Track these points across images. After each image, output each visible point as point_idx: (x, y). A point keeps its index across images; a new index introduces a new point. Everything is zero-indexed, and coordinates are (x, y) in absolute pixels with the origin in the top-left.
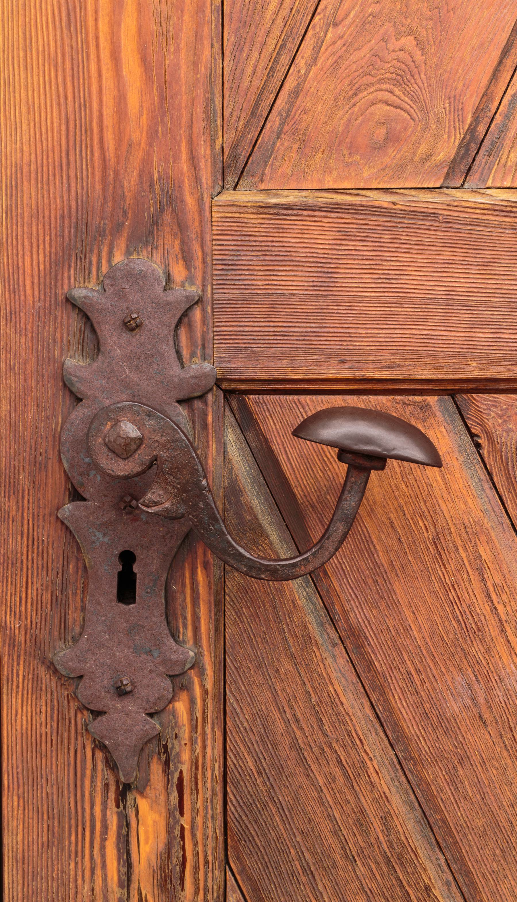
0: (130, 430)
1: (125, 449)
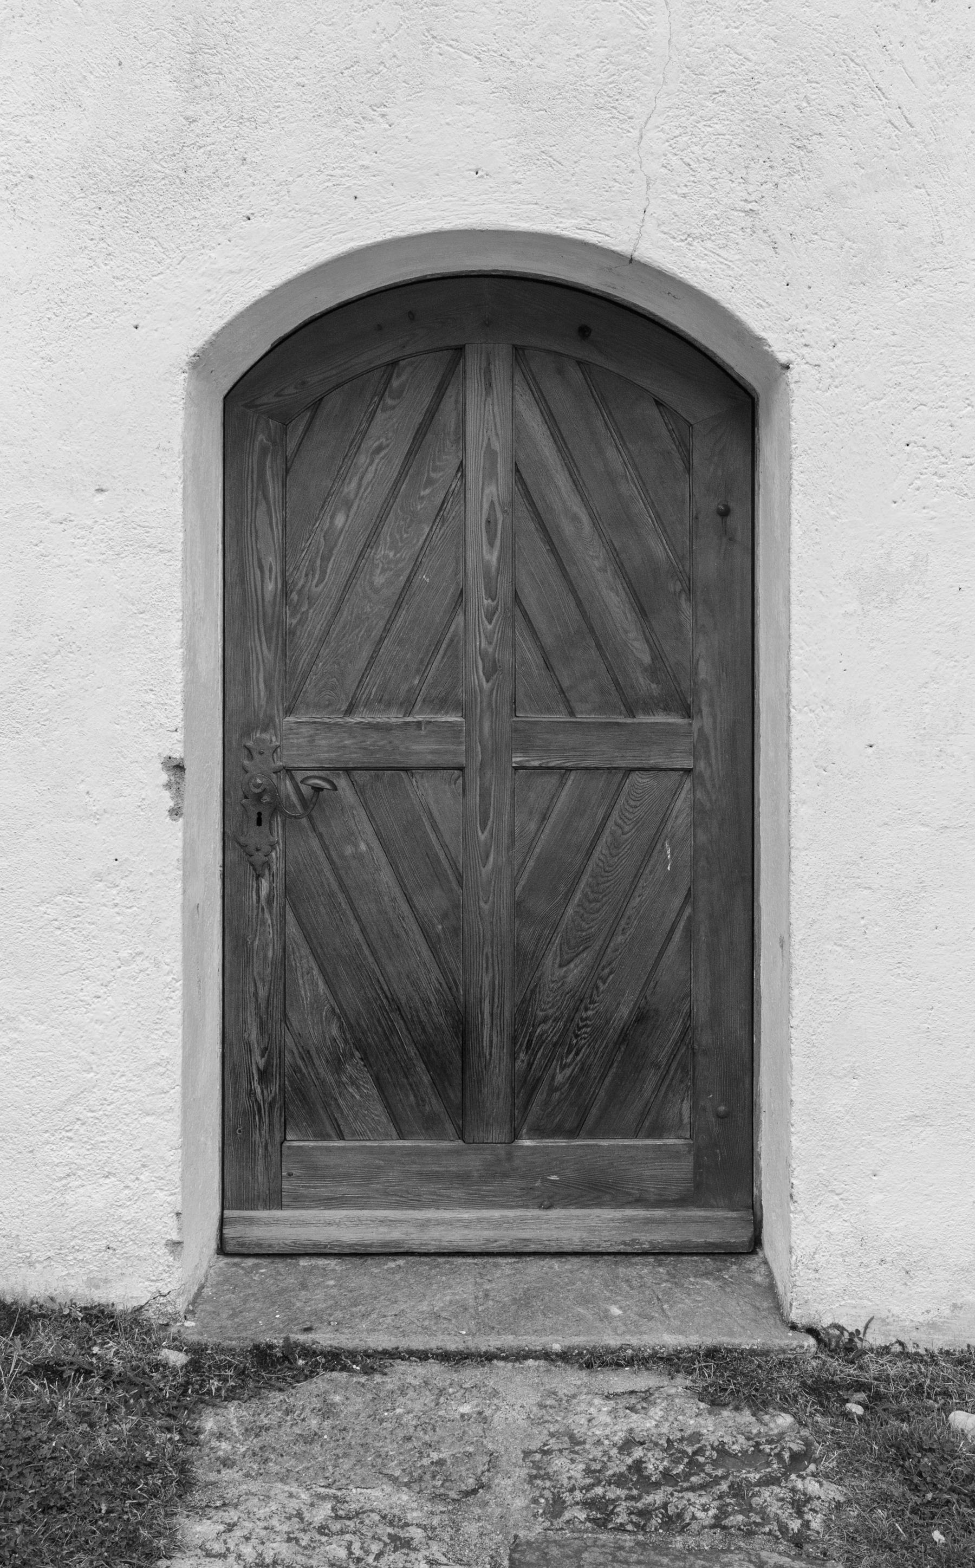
0: (259, 781)
1: (258, 786)
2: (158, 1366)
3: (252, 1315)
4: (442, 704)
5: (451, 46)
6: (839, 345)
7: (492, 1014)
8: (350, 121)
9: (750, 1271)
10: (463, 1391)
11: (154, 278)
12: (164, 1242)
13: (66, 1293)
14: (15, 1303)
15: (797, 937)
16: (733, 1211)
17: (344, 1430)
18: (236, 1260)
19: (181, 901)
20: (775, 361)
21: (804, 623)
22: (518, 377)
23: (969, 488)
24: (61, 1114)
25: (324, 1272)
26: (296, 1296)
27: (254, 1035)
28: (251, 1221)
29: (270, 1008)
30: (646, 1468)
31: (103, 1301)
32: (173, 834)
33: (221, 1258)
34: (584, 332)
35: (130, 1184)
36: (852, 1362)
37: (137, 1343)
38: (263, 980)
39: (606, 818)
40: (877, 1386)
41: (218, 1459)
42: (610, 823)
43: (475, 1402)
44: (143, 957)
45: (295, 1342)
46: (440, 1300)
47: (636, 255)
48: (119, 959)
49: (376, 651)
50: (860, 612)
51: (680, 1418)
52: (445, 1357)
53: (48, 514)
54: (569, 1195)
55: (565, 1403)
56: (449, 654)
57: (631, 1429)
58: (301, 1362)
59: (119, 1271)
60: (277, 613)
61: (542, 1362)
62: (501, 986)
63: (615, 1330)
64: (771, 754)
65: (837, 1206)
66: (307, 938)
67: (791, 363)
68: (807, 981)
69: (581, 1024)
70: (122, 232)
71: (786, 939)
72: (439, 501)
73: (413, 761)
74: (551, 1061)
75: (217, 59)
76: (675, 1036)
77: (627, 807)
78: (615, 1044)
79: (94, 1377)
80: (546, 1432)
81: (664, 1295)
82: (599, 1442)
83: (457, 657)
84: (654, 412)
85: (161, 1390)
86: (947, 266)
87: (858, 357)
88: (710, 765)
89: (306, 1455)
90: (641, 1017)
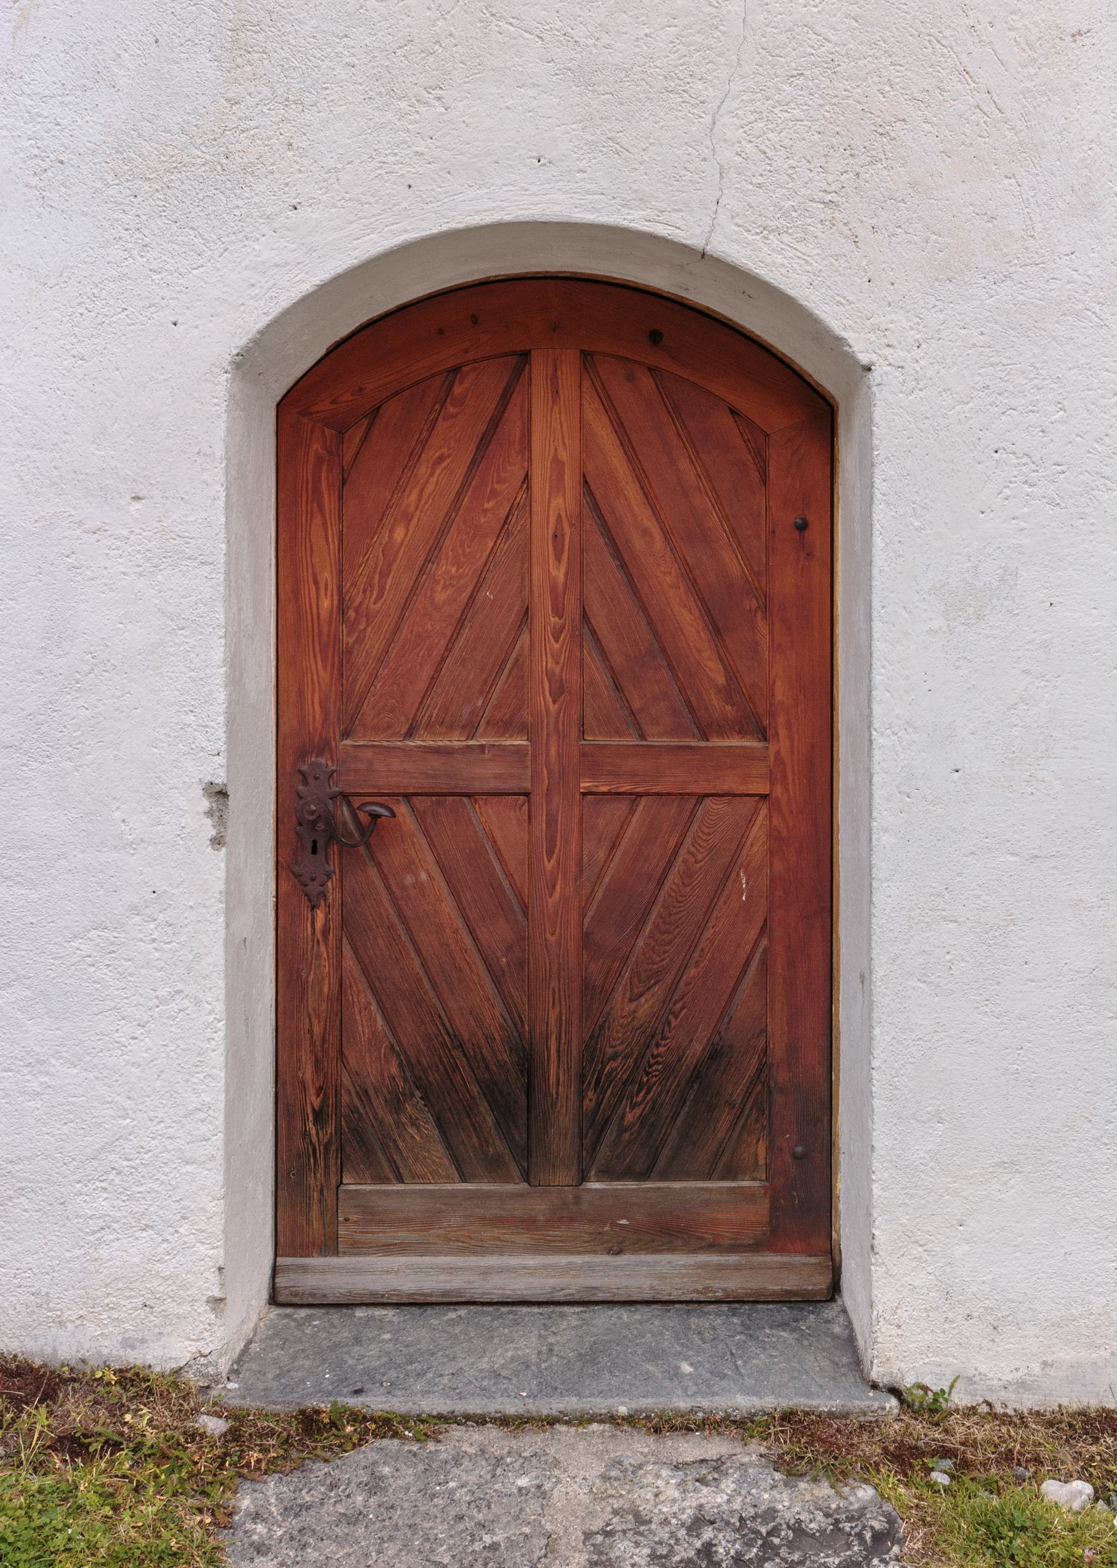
0: (313, 808)
1: (313, 812)
2: (193, 1436)
3: (300, 1374)
4: (506, 726)
5: (511, 24)
6: (924, 346)
7: (558, 1051)
8: (403, 105)
9: (828, 1321)
10: (521, 1460)
11: (194, 272)
12: (205, 1298)
13: (100, 1354)
14: (44, 1365)
15: (879, 973)
16: (810, 1256)
17: (392, 1507)
18: (289, 1311)
19: (224, 936)
20: (856, 362)
21: (886, 641)
22: (587, 384)
23: (1062, 498)
24: (95, 1163)
25: (381, 1324)
26: (348, 1353)
27: (308, 1073)
28: (305, 1269)
29: (326, 1046)
30: (716, 1552)
31: (139, 1363)
32: (215, 866)
33: (273, 1308)
34: (655, 337)
35: (169, 1237)
36: (937, 1424)
37: (175, 1408)
38: (319, 1016)
39: (679, 845)
40: (964, 1452)
41: (251, 1544)
42: (683, 852)
43: (534, 1474)
44: (183, 995)
45: (343, 1406)
46: (500, 1357)
47: (709, 249)
48: (157, 997)
49: (438, 671)
50: (945, 629)
51: (754, 1491)
52: (504, 1421)
53: (80, 523)
54: (640, 1240)
55: (632, 1473)
56: (513, 674)
57: (701, 1506)
58: (349, 1429)
59: (157, 1330)
60: (333, 630)
61: (607, 1426)
62: (569, 1022)
63: (685, 1390)
64: (852, 779)
65: (921, 1258)
66: (365, 971)
67: (873, 364)
68: (889, 1019)
69: (652, 1061)
70: (159, 222)
71: (867, 974)
72: (503, 513)
73: (478, 786)
74: (620, 1100)
75: (261, 37)
76: (750, 1072)
77: (700, 834)
78: (687, 1083)
79: (123, 1449)
80: (609, 1509)
81: (738, 1349)
82: (665, 1522)
83: (522, 677)
84: (728, 421)
85: (196, 1463)
86: (1039, 261)
87: (943, 358)
88: (788, 790)
89: (349, 1538)
90: (716, 1054)
